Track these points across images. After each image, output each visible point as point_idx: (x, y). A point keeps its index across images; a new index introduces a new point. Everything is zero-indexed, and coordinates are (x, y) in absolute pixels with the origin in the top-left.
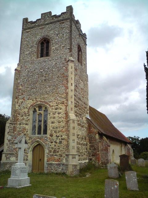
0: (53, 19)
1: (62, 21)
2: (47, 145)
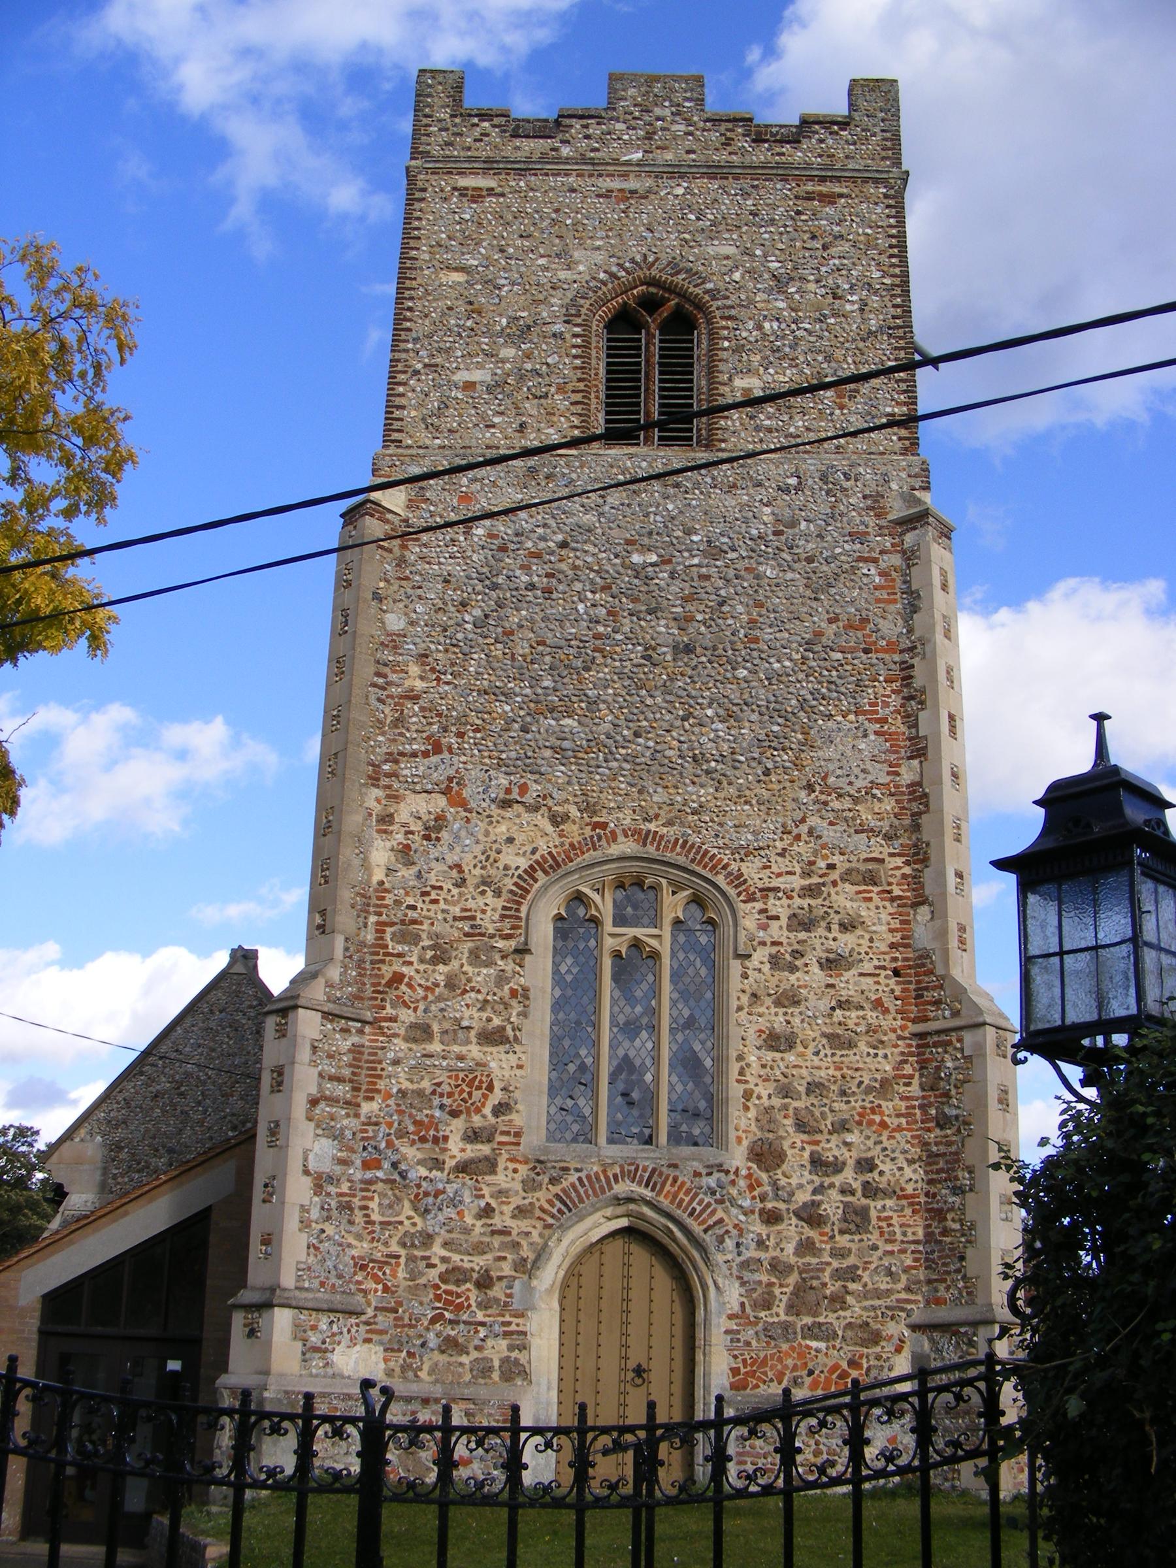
0: (728, 143)
1: (823, 179)
2: (729, 1243)
